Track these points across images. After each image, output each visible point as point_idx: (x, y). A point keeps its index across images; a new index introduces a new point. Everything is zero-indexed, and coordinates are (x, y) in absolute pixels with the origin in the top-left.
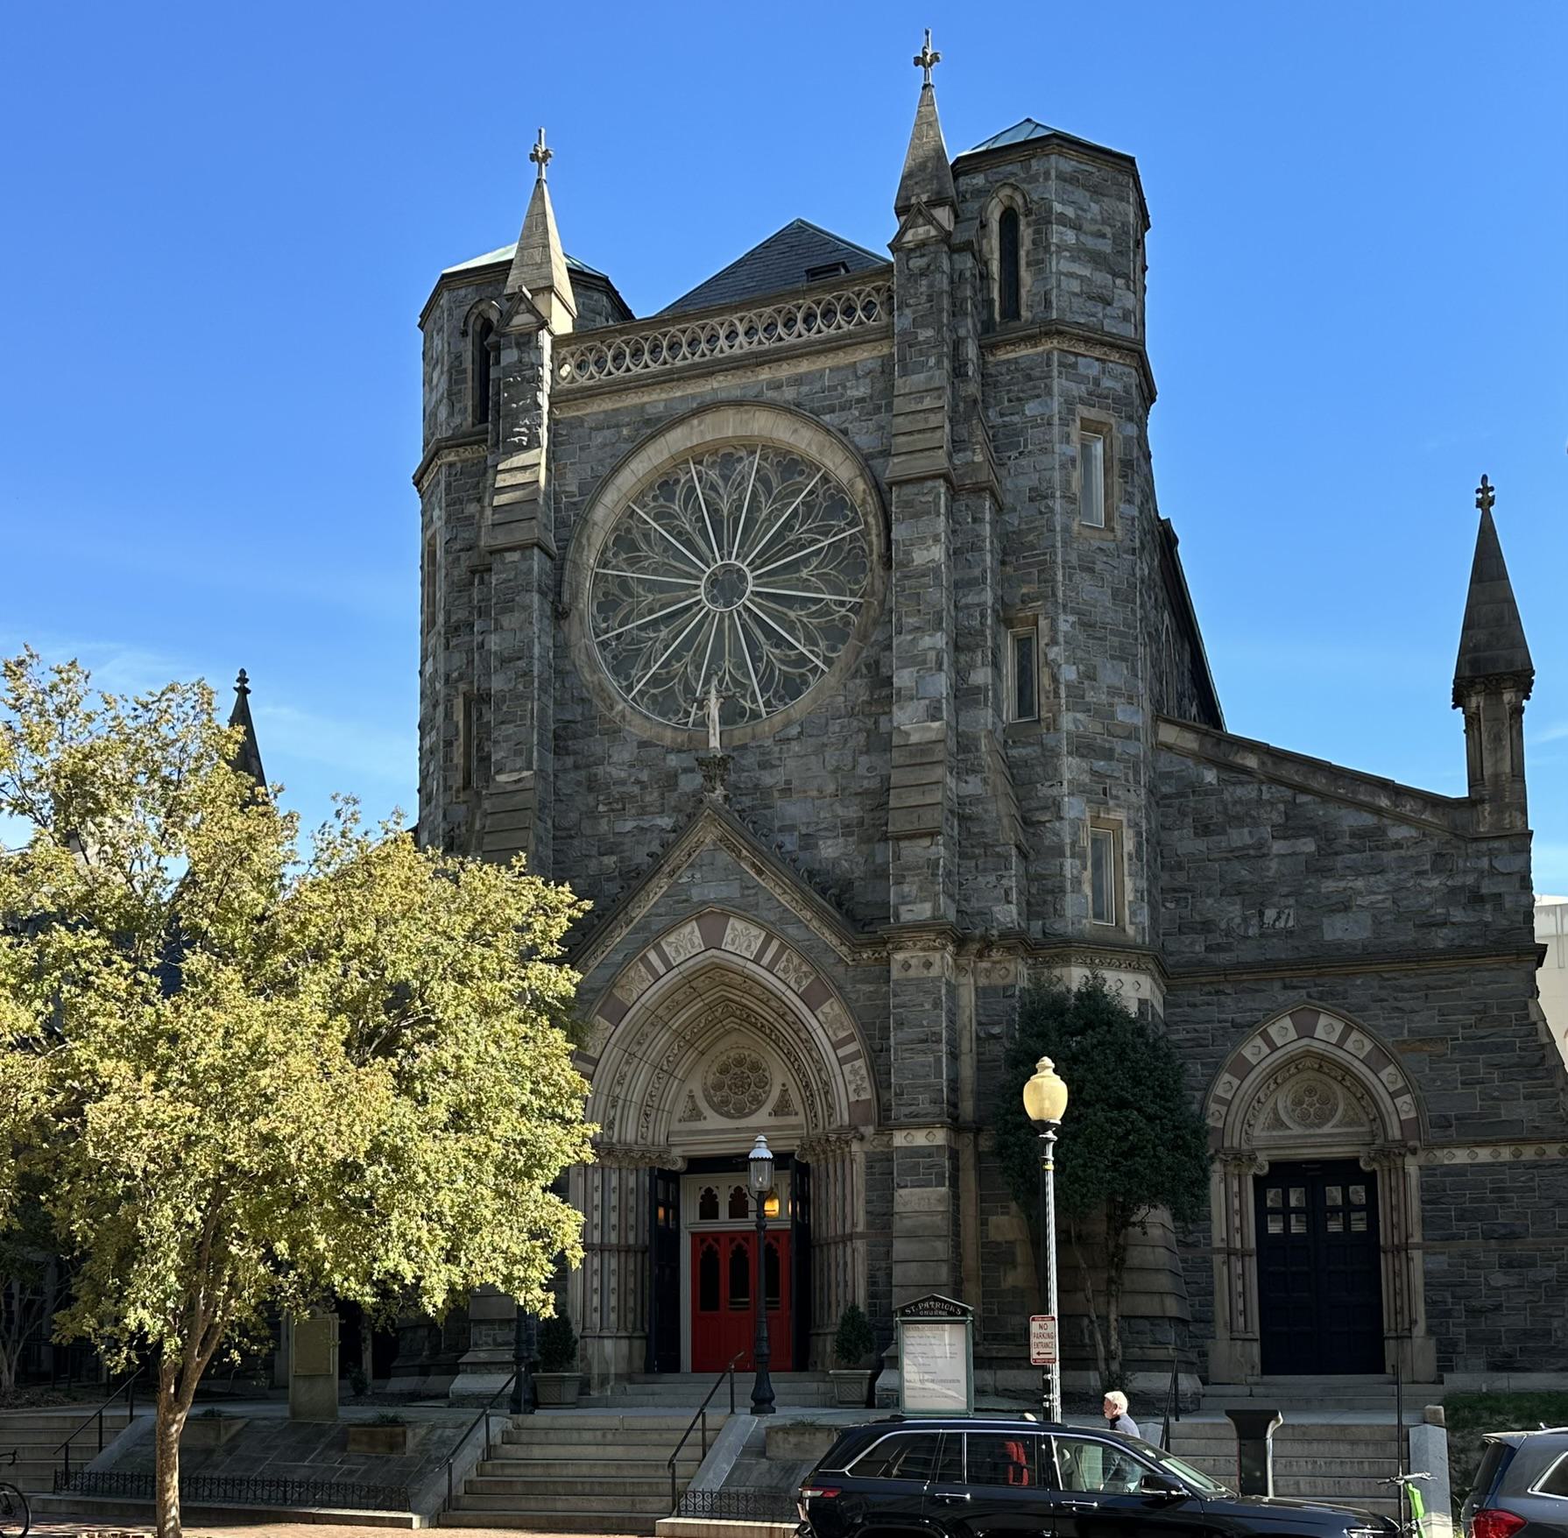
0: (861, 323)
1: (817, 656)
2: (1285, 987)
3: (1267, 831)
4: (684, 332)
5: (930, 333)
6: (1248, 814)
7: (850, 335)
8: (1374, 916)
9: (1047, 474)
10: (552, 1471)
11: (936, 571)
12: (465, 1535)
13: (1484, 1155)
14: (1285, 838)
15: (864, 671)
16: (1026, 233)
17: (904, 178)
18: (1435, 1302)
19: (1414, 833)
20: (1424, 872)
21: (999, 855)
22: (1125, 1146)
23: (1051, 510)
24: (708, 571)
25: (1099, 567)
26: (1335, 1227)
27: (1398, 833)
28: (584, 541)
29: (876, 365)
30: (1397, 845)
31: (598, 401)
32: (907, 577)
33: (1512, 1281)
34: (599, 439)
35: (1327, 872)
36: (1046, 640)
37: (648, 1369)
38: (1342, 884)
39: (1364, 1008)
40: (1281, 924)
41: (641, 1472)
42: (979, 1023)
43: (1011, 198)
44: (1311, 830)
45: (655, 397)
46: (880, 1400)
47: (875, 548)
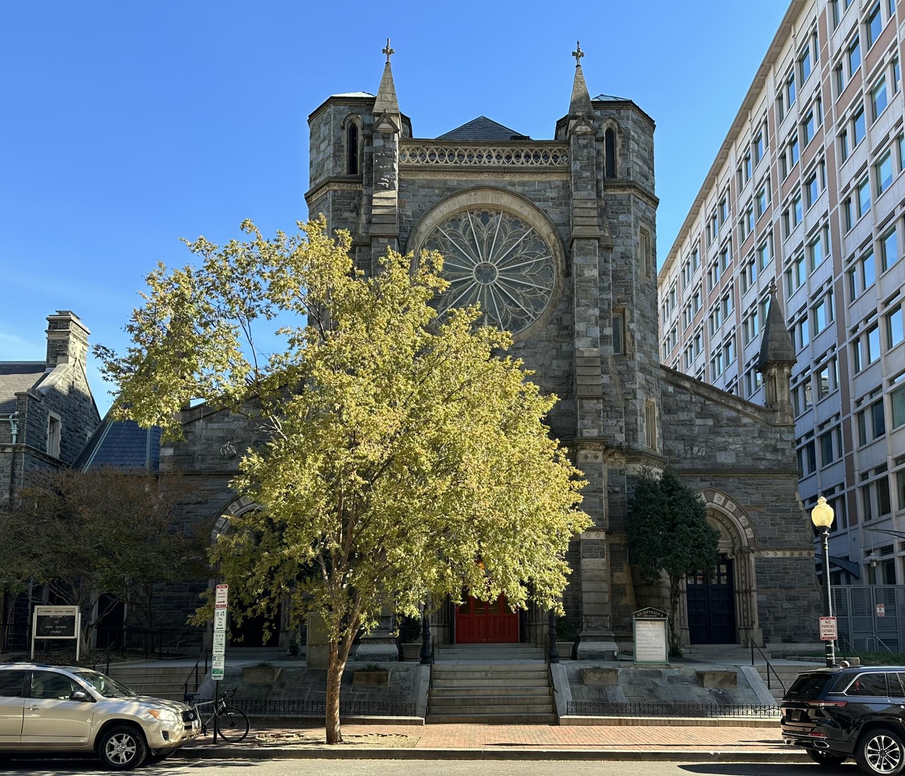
0: (551, 164)
1: (530, 312)
2: (702, 480)
3: (693, 415)
4: (466, 150)
5: (588, 174)
6: (686, 407)
7: (546, 168)
8: (736, 454)
9: (629, 247)
10: (470, 693)
11: (595, 280)
12: (685, 731)
13: (780, 554)
14: (701, 418)
15: (555, 321)
16: (619, 141)
17: (572, 103)
18: (762, 614)
19: (751, 421)
20: (756, 437)
21: (617, 411)
22: (697, 543)
23: (631, 264)
24: (477, 265)
25: (646, 292)
26: (714, 582)
27: (746, 420)
28: (415, 240)
29: (560, 184)
30: (745, 425)
31: (423, 173)
32: (581, 281)
33: (791, 606)
34: (423, 192)
35: (718, 434)
36: (629, 320)
37: (445, 643)
38: (724, 439)
39: (733, 491)
40: (700, 454)
41: (519, 693)
42: (609, 486)
43: (612, 124)
44: (712, 416)
45: (452, 178)
46: (580, 656)
47: (560, 266)
